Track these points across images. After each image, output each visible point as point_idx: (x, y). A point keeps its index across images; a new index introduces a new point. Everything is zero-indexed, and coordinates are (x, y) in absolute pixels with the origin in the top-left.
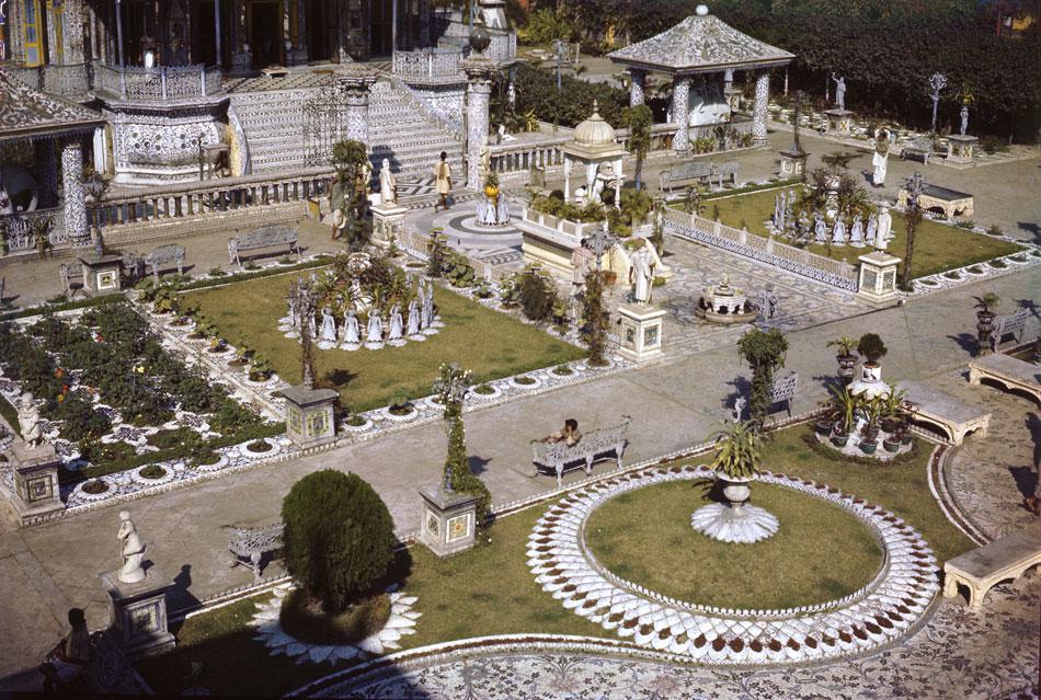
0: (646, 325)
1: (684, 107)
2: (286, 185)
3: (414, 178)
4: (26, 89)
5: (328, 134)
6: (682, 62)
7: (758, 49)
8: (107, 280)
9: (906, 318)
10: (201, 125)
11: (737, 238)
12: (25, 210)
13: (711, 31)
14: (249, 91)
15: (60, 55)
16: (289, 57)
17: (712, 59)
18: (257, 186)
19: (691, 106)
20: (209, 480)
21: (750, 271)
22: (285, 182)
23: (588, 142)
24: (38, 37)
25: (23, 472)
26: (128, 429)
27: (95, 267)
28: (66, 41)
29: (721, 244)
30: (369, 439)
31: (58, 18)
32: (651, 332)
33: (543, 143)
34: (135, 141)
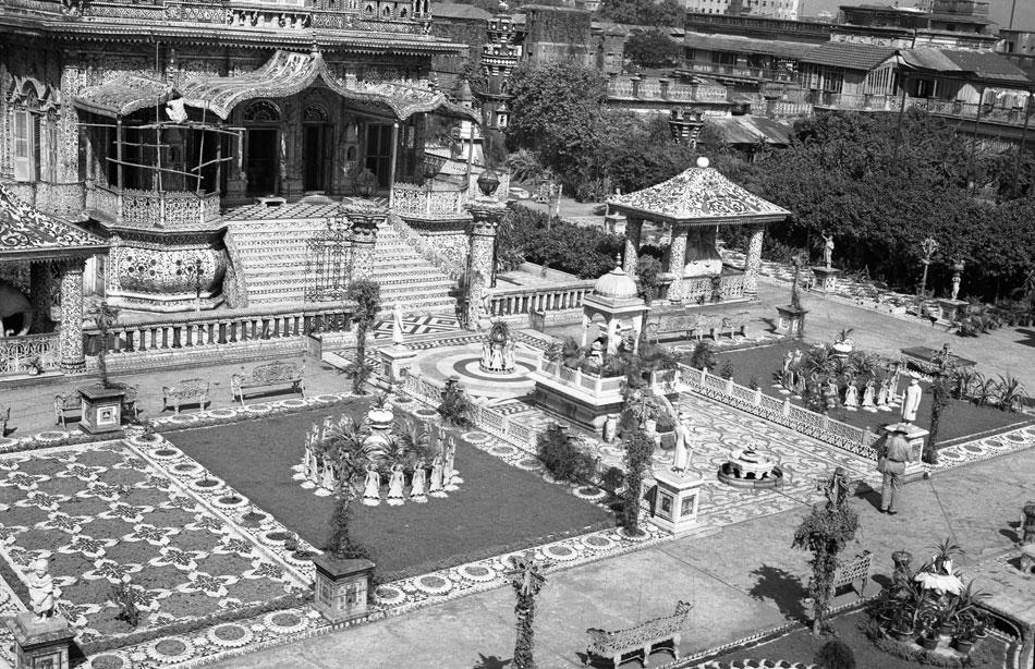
0: (683, 495)
1: (681, 259)
2: (287, 319)
3: (411, 316)
4: (28, 209)
5: (325, 267)
6: (682, 212)
7: (755, 204)
8: (107, 415)
9: (935, 492)
10: (197, 251)
11: (752, 397)
12: (15, 334)
13: (710, 184)
14: (245, 219)
15: (52, 172)
16: (285, 186)
17: (712, 212)
18: (259, 319)
19: (687, 262)
20: (233, 656)
21: (766, 434)
22: (287, 316)
23: (611, 295)
24: (29, 152)
25: (27, 649)
26: (87, 540)
27: (93, 402)
28: (60, 159)
29: (733, 403)
30: (402, 614)
31: (53, 134)
32: (689, 501)
33: (542, 287)
34: (129, 264)
